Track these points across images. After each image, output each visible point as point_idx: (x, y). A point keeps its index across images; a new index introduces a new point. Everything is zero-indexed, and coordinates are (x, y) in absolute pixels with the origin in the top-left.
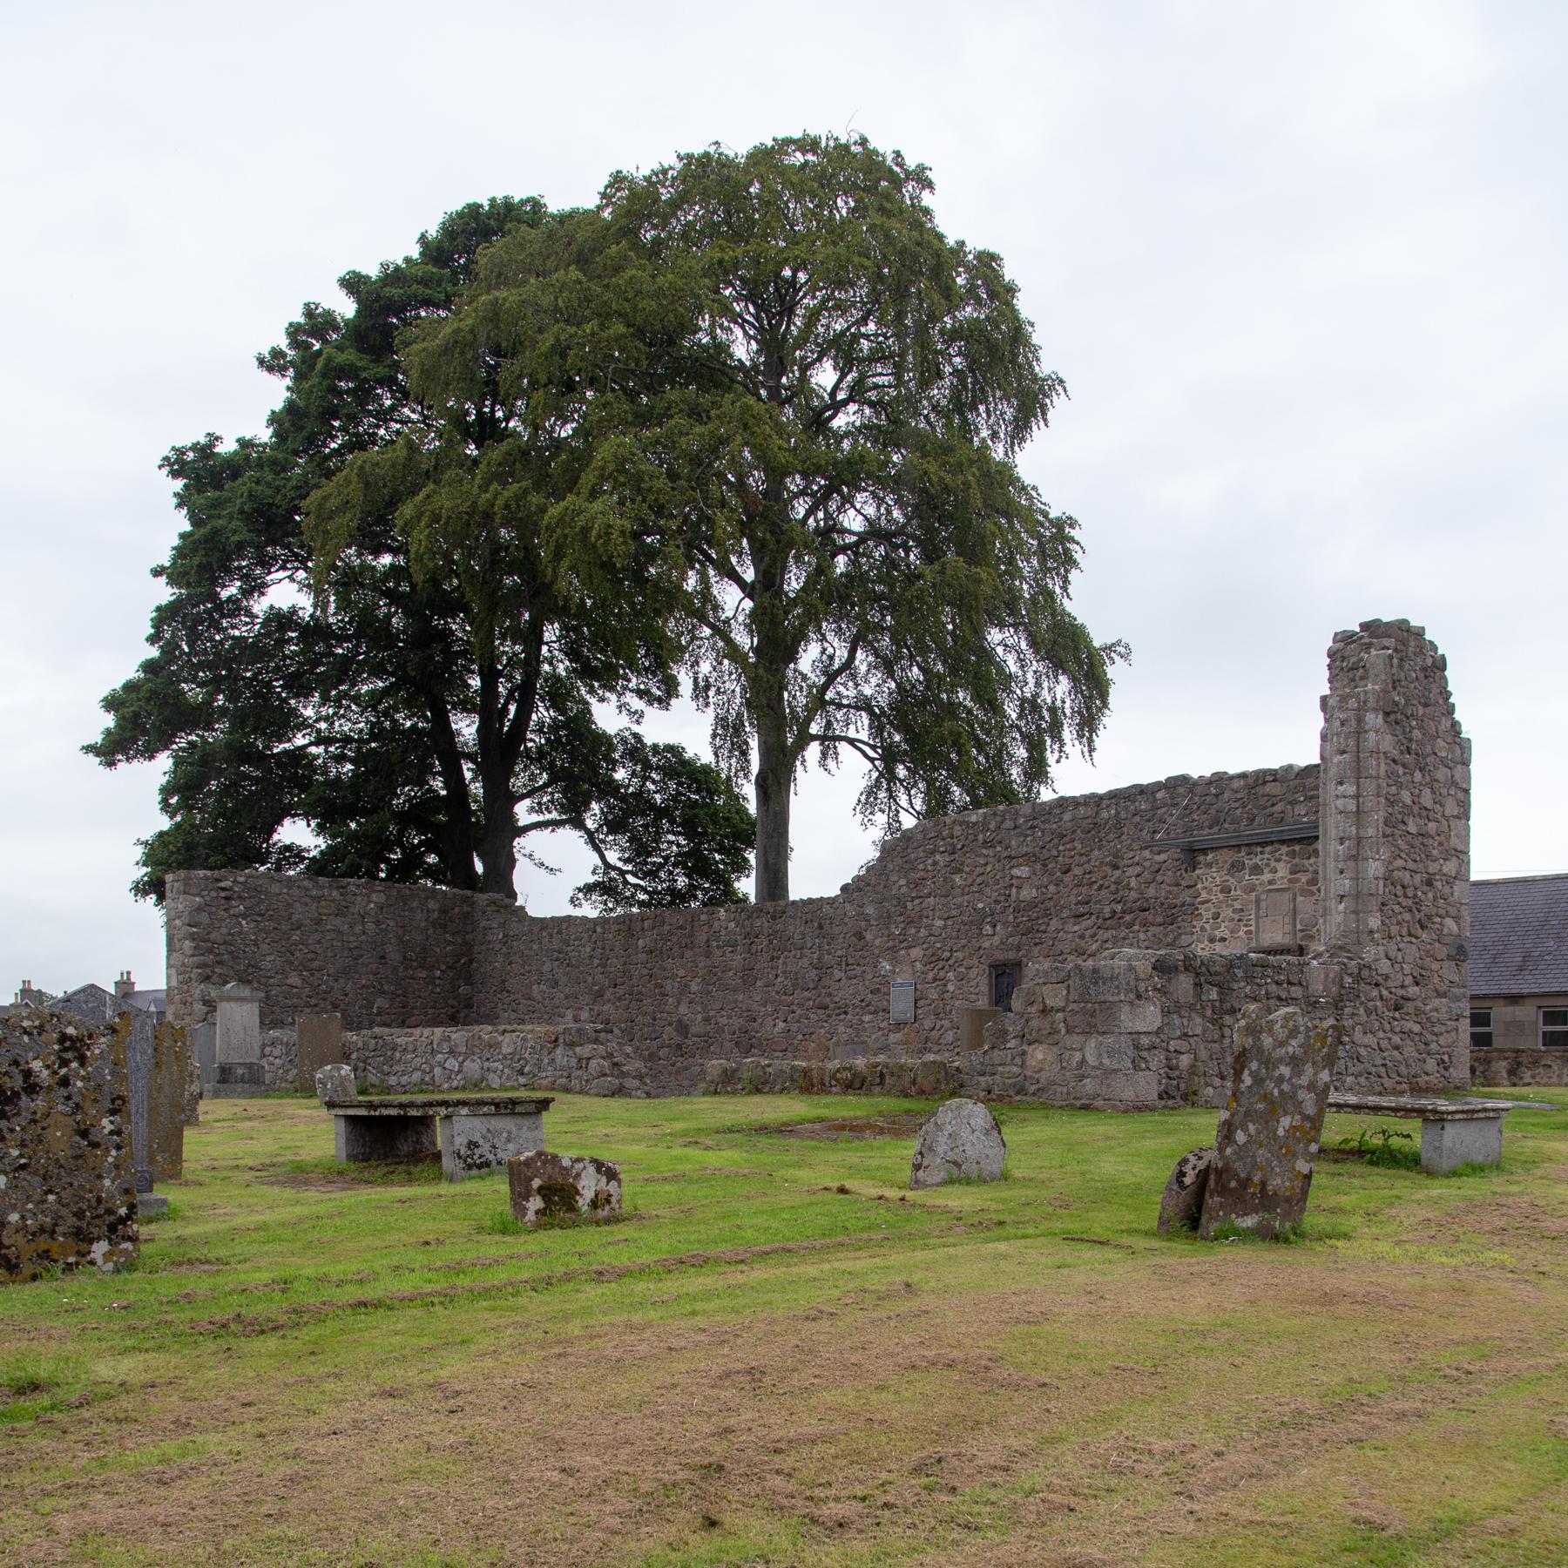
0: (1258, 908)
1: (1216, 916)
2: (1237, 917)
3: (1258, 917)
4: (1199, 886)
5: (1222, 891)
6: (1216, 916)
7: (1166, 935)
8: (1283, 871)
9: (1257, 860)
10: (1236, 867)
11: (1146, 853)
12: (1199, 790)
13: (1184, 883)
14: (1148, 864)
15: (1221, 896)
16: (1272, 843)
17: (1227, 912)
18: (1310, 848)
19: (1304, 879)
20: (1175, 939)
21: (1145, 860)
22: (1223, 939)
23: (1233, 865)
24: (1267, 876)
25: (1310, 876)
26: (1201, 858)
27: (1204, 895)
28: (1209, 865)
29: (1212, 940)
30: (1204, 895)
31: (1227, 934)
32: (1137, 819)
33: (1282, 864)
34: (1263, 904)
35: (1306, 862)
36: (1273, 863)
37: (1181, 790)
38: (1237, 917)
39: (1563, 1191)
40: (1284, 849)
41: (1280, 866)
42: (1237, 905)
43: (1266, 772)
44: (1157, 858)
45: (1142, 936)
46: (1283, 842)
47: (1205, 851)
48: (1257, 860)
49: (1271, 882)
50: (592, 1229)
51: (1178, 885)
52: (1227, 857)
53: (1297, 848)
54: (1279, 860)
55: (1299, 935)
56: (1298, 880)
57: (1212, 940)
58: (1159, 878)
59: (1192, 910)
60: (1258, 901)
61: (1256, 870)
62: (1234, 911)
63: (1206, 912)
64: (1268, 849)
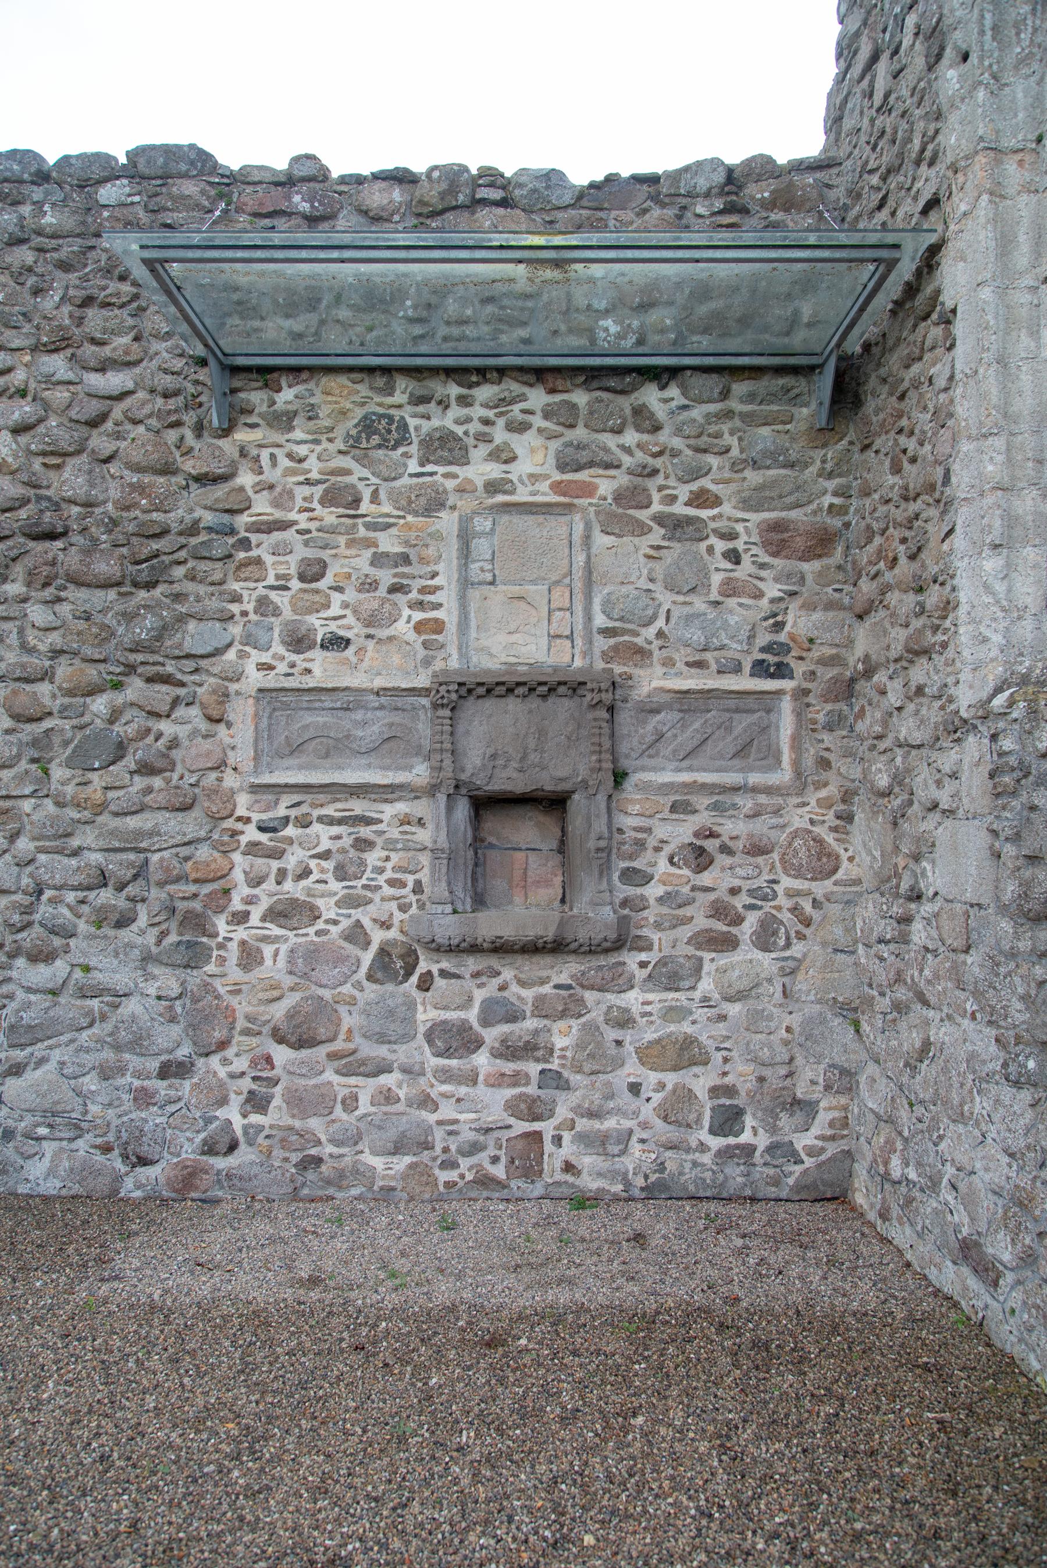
0: (466, 554)
1: (312, 572)
2: (386, 577)
3: (465, 583)
4: (246, 479)
5: (328, 500)
6: (312, 572)
7: (129, 617)
8: (533, 460)
9: (447, 421)
10: (378, 434)
11: (57, 364)
12: (249, 197)
13: (189, 466)
14: (60, 396)
15: (330, 516)
16: (502, 372)
17: (350, 563)
18: (625, 403)
19: (606, 487)
20: (163, 631)
21: (51, 382)
22: (337, 643)
23: (367, 426)
24: (480, 469)
25: (622, 479)
26: (257, 398)
27: (262, 506)
28: (283, 421)
29: (299, 642)
30: (262, 506)
31: (353, 629)
32: (25, 255)
33: (530, 438)
34: (482, 547)
35: (610, 441)
36: (500, 435)
37: (190, 188)
38: (386, 577)
39: (2, 1056)
40: (537, 398)
41: (520, 443)
42: (388, 543)
43: (490, 176)
44: (95, 380)
45: (38, 614)
46: (539, 375)
47: (267, 375)
48: (447, 421)
49: (493, 487)
50: (489, 704)
51: (167, 470)
52: (345, 400)
53: (580, 398)
54: (521, 428)
55: (602, 644)
56: (588, 490)
57: (299, 642)
58: (100, 442)
59: (226, 545)
60: (466, 537)
61: (445, 448)
62: (378, 560)
63: (278, 559)
64: (485, 392)
